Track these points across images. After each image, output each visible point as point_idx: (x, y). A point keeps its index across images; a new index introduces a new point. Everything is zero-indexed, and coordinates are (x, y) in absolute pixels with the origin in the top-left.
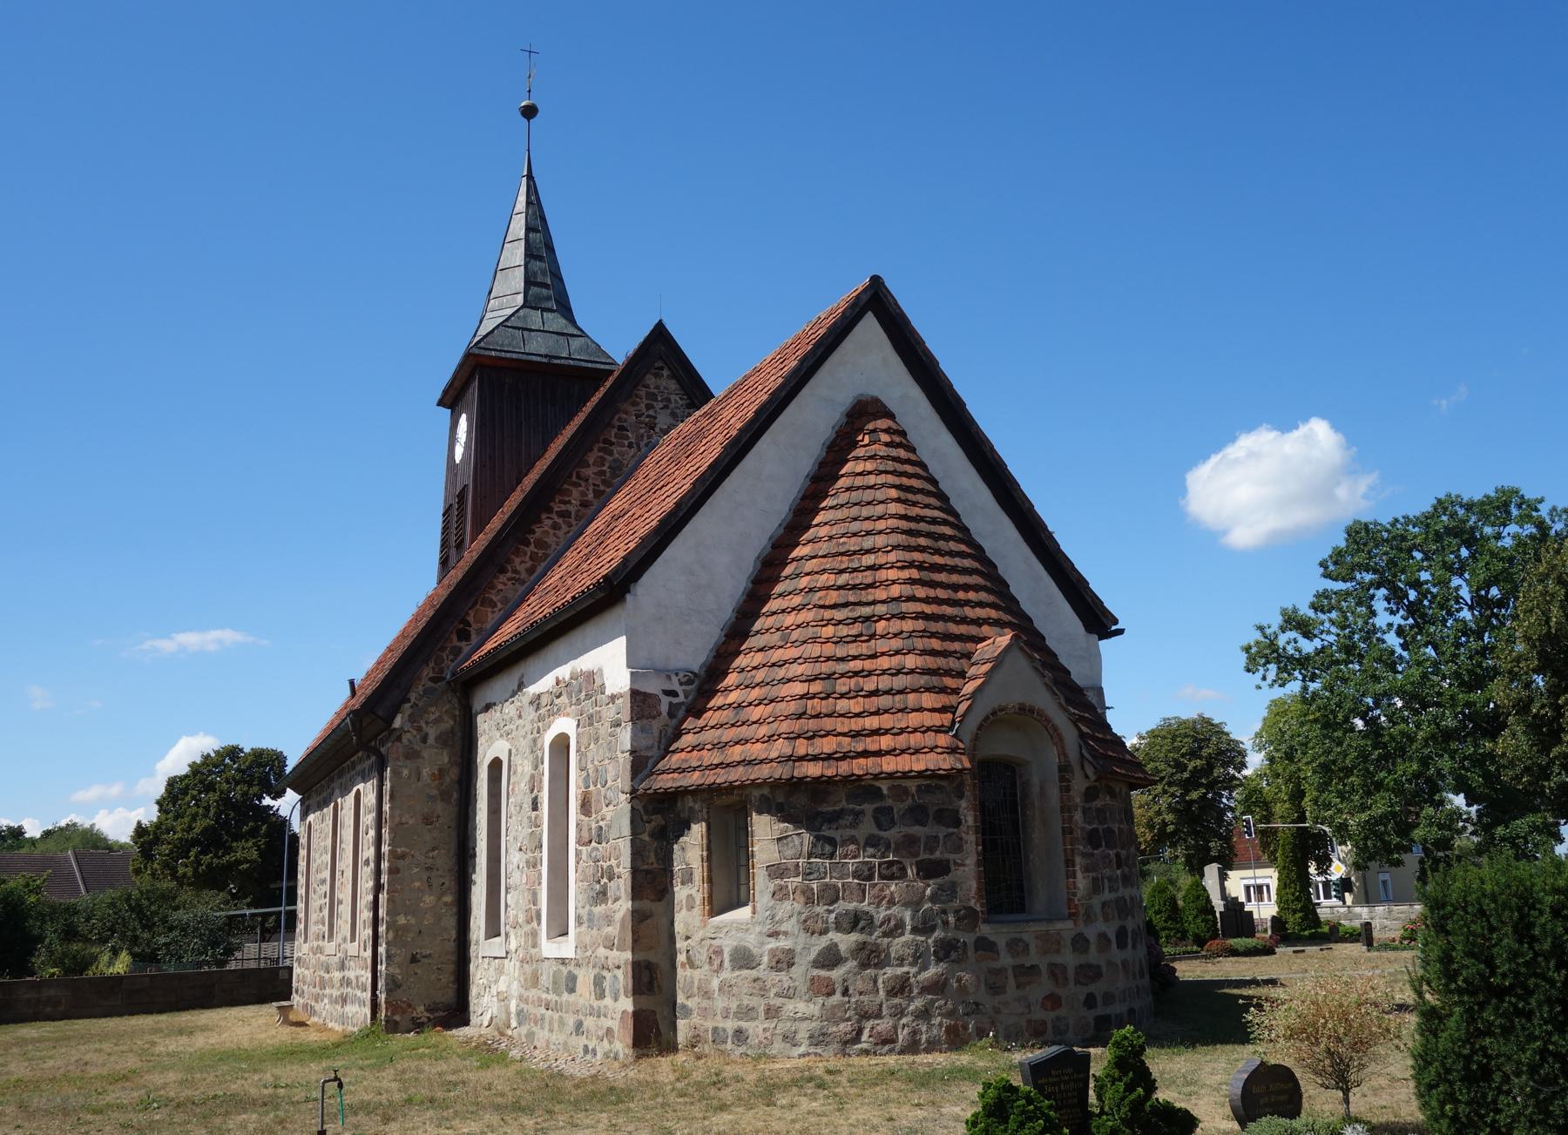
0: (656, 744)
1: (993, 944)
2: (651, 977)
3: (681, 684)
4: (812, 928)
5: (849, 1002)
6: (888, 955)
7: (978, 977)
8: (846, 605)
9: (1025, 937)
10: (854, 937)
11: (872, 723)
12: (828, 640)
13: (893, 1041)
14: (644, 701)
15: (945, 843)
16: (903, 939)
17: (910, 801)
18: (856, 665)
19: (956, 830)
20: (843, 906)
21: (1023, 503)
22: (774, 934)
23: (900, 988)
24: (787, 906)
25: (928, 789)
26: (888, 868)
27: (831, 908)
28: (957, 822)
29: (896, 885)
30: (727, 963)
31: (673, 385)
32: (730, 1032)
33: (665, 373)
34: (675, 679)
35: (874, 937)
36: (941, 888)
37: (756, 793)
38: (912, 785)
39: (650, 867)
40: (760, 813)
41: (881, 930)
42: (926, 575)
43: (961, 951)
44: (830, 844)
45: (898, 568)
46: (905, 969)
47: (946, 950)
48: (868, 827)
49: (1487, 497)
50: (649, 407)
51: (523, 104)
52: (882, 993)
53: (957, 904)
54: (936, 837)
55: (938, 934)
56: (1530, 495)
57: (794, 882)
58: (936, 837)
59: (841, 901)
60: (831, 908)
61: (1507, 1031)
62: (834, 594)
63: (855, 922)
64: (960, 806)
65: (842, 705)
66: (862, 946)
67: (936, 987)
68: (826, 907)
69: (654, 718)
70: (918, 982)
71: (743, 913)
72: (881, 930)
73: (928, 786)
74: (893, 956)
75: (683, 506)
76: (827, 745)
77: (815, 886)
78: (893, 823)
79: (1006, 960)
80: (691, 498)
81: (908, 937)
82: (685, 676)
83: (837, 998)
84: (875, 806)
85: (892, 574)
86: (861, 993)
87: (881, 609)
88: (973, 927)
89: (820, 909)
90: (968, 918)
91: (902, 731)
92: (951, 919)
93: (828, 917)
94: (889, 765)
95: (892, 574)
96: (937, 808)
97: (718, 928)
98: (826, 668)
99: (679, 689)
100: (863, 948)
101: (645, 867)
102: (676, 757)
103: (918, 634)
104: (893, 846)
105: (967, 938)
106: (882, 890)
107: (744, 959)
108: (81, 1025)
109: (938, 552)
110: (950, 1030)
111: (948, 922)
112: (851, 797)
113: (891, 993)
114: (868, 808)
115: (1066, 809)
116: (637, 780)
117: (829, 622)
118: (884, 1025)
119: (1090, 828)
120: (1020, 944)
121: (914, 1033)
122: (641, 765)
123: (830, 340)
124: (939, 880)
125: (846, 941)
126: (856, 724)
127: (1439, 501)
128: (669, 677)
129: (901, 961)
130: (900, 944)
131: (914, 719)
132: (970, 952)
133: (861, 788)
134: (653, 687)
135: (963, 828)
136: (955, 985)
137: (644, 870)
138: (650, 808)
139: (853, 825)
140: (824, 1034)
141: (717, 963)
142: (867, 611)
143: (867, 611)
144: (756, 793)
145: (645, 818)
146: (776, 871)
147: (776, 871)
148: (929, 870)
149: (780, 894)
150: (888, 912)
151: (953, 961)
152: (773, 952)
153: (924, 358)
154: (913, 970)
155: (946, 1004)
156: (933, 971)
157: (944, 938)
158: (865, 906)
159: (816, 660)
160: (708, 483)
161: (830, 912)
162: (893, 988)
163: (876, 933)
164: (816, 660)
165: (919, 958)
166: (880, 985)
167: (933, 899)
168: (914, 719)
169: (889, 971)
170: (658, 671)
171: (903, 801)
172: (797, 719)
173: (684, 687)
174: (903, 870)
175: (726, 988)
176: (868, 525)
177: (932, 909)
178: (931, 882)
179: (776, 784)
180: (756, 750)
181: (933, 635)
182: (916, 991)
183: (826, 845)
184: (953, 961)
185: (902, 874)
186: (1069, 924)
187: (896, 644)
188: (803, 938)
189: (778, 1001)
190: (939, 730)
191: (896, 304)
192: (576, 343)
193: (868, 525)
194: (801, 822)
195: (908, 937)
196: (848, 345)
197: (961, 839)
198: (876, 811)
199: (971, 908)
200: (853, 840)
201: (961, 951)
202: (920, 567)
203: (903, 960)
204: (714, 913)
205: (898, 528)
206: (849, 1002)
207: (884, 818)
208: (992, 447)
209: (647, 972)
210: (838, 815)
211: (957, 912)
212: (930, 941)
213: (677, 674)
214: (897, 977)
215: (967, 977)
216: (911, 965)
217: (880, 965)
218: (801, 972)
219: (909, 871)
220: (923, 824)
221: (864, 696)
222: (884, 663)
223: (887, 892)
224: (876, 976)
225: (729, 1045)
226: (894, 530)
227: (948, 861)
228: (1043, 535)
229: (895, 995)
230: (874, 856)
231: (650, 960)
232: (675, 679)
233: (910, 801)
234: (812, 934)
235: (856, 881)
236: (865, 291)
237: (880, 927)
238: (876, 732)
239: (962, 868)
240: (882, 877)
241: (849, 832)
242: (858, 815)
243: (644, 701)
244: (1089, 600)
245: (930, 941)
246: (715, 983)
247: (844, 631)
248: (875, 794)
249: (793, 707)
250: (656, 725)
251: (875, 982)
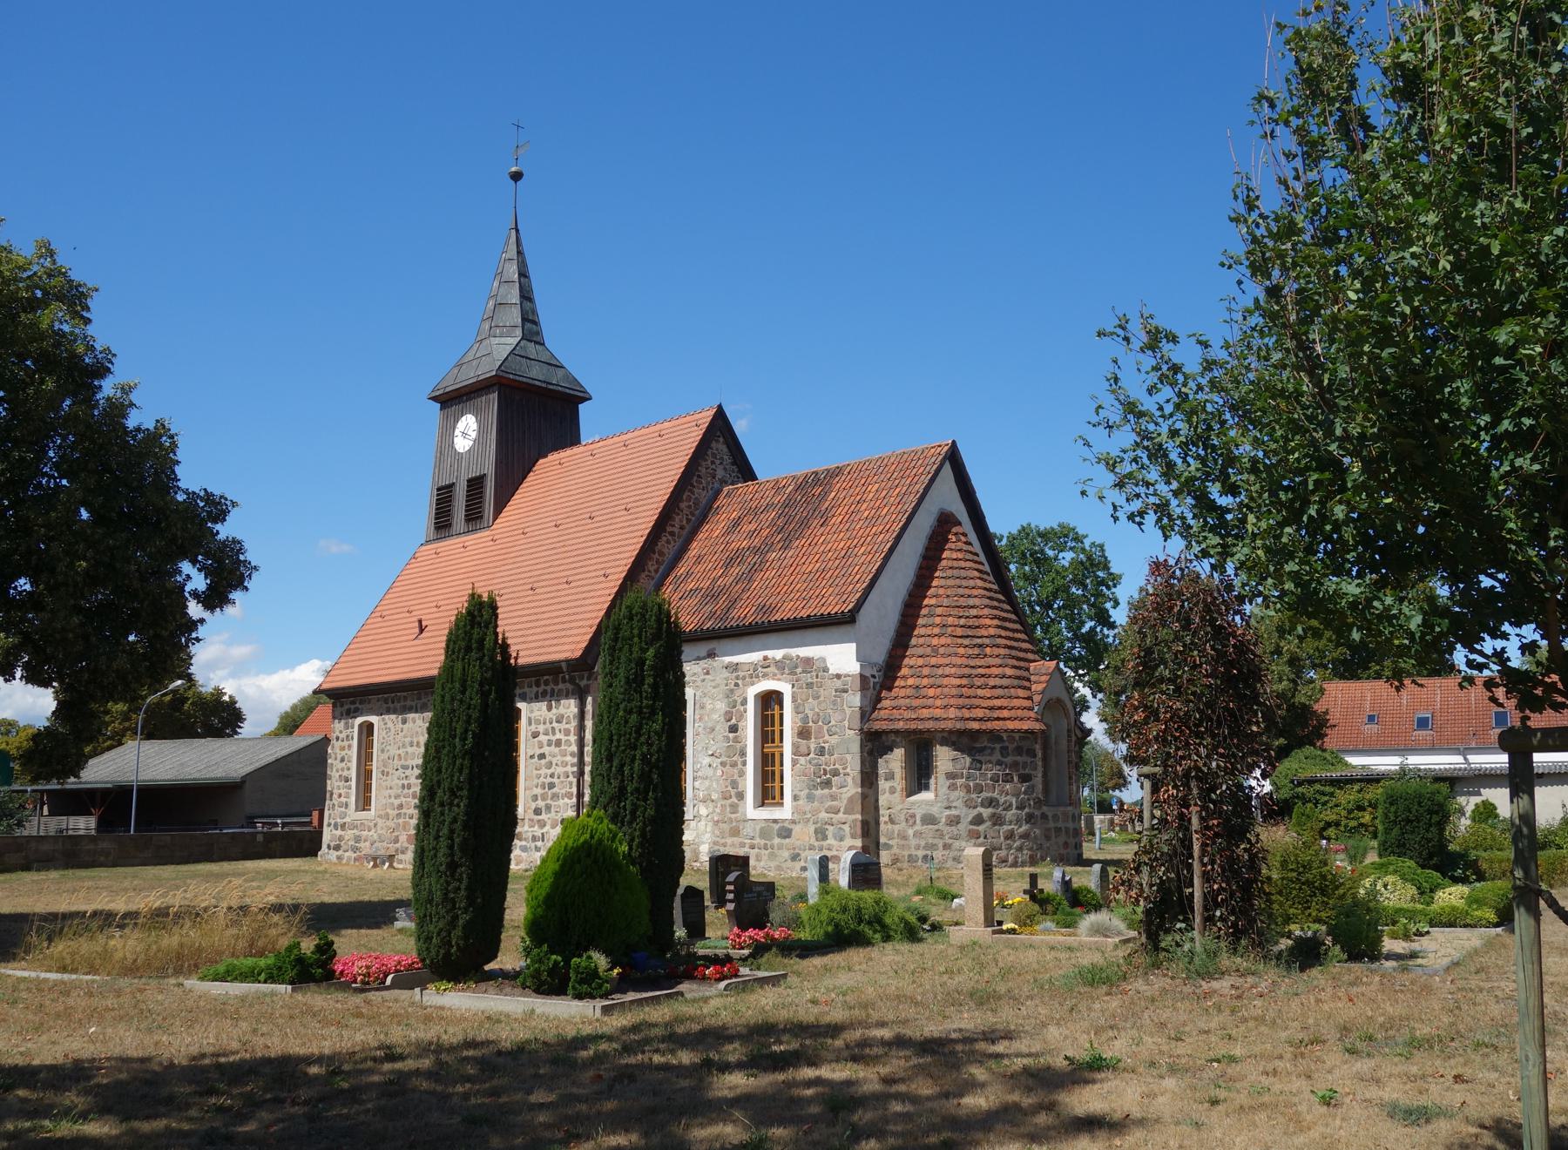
4: (969, 805)
8: (967, 637)
10: (990, 810)
11: (998, 703)
12: (963, 656)
13: (1006, 861)
18: (981, 671)
20: (984, 794)
22: (949, 808)
23: (1010, 836)
24: (956, 793)
28: (1035, 756)
30: (918, 821)
31: (725, 449)
32: (920, 857)
33: (721, 439)
36: (1028, 787)
37: (940, 735)
38: (1017, 736)
40: (941, 745)
47: (1030, 818)
48: (997, 756)
49: (1053, 529)
50: (713, 463)
56: (1081, 531)
57: (960, 782)
61: (1413, 832)
62: (959, 629)
63: (991, 803)
65: (980, 692)
66: (994, 815)
67: (1025, 836)
76: (979, 713)
81: (1014, 811)
85: (988, 622)
87: (987, 641)
88: (1040, 808)
89: (974, 796)
90: (1038, 803)
91: (1013, 708)
94: (1010, 725)
95: (988, 622)
97: (913, 803)
98: (967, 671)
102: (882, 712)
107: (929, 820)
108: (226, 866)
110: (1031, 857)
112: (990, 740)
113: (1007, 838)
114: (998, 746)
117: (961, 645)
118: (1003, 853)
121: (1016, 857)
122: (865, 714)
125: (986, 812)
127: (1023, 528)
129: (1010, 824)
130: (1011, 814)
131: (1016, 703)
133: (994, 736)
139: (990, 755)
141: (911, 822)
142: (979, 641)
143: (979, 641)
144: (940, 735)
146: (950, 776)
147: (950, 776)
148: (1025, 778)
149: (952, 787)
152: (948, 817)
156: (1025, 828)
158: (995, 795)
159: (960, 666)
164: (960, 666)
165: (1018, 821)
167: (1025, 793)
168: (1016, 703)
169: (1006, 828)
175: (917, 834)
176: (967, 592)
179: (951, 732)
180: (938, 713)
181: (1013, 658)
183: (977, 764)
185: (1012, 781)
187: (998, 661)
188: (965, 810)
189: (951, 841)
192: (560, 372)
193: (967, 592)
195: (1014, 811)
200: (990, 762)
204: (909, 795)
215: (1037, 831)
217: (1001, 825)
218: (964, 827)
222: (995, 671)
225: (920, 863)
226: (983, 596)
241: (988, 758)
246: (910, 832)
247: (970, 652)
248: (1000, 739)
249: (954, 691)
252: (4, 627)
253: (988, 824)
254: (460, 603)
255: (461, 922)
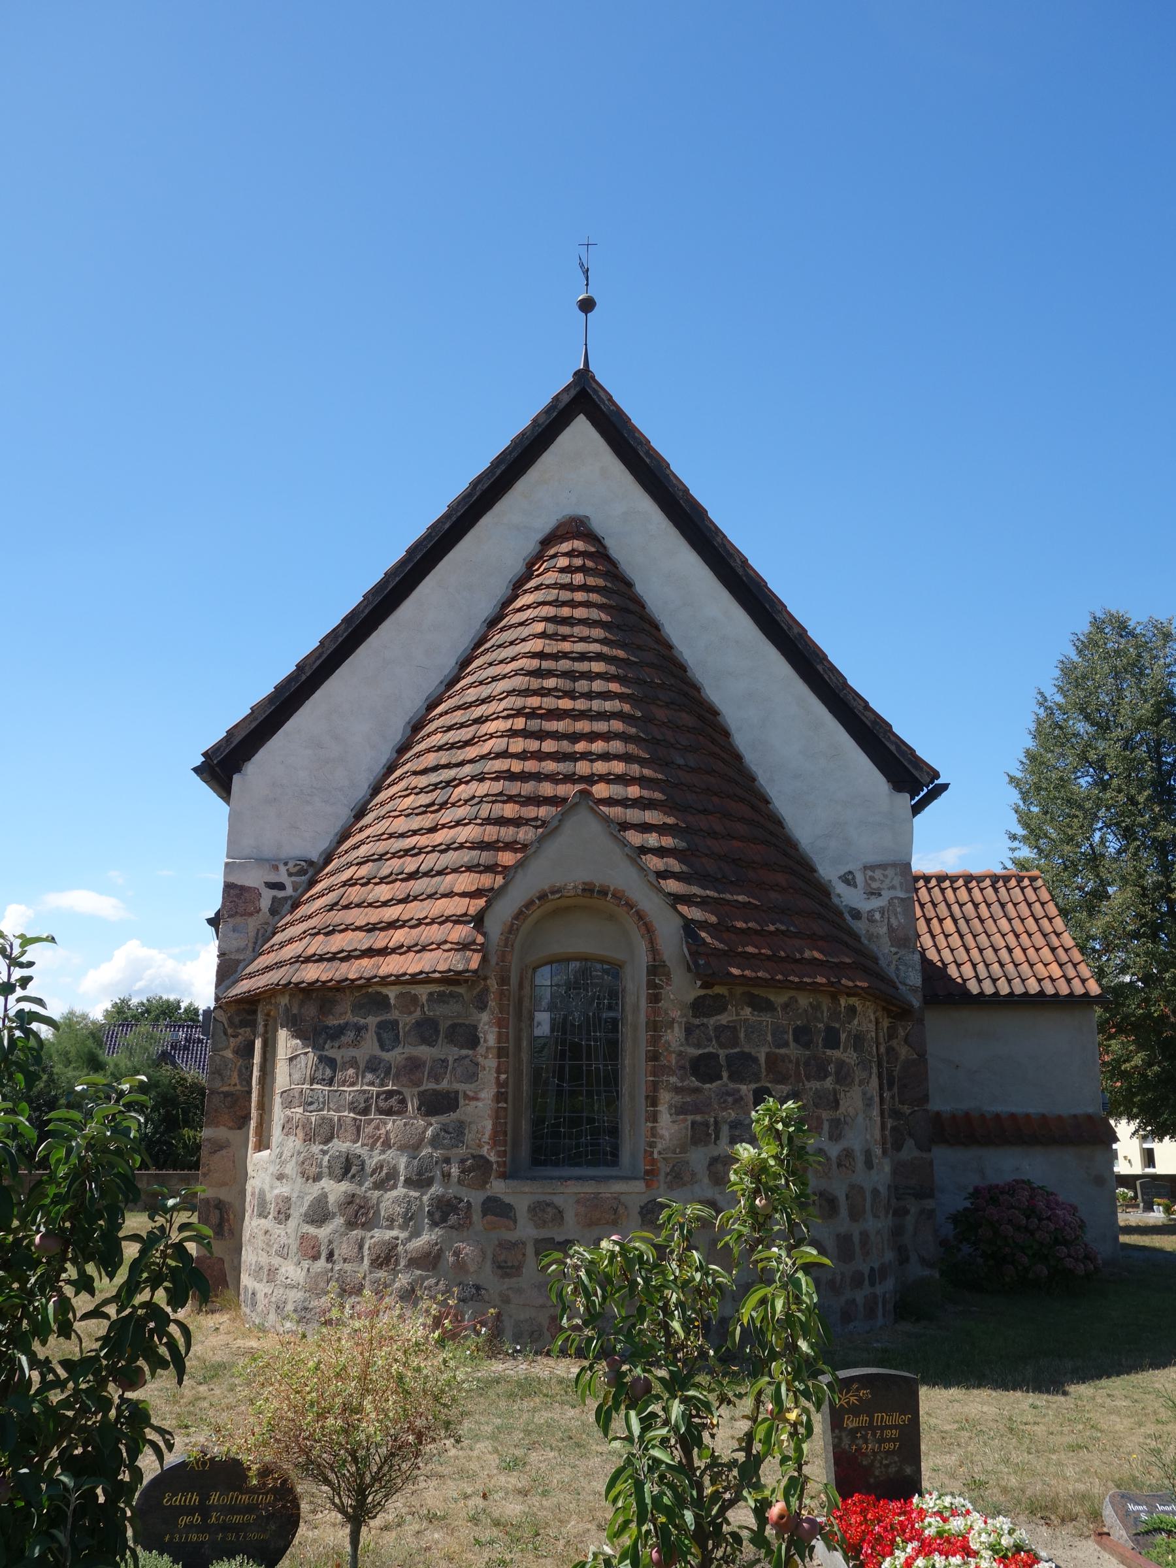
0: (251, 945)
1: (510, 1207)
2: (222, 1218)
3: (290, 875)
5: (332, 1269)
6: (377, 1212)
7: (483, 1252)
9: (558, 1200)
10: (345, 1186)
14: (239, 896)
15: (454, 1069)
16: (394, 1193)
17: (418, 1013)
19: (470, 1052)
20: (340, 1146)
21: (790, 628)
22: (280, 1177)
23: (385, 1258)
25: (441, 998)
26: (386, 1100)
27: (325, 1148)
28: (473, 1041)
29: (394, 1121)
34: (283, 869)
35: (363, 1189)
39: (232, 1089)
41: (372, 1180)
42: (534, 725)
43: (462, 1214)
44: (330, 1068)
45: (503, 718)
46: (395, 1233)
47: (443, 1211)
48: (369, 1047)
51: (580, 298)
52: (366, 1262)
53: (462, 1151)
54: (445, 1061)
55: (436, 1189)
58: (445, 1061)
59: (336, 1140)
60: (325, 1148)
63: (347, 1168)
64: (479, 1021)
66: (350, 1199)
67: (428, 1261)
68: (321, 1147)
69: (251, 914)
70: (406, 1251)
71: (266, 1153)
72: (372, 1180)
73: (441, 994)
74: (382, 1214)
75: (307, 668)
77: (313, 1119)
78: (396, 1041)
79: (526, 1230)
80: (318, 658)
81: (400, 1191)
82: (296, 865)
83: (322, 1263)
84: (379, 1019)
86: (345, 1260)
88: (483, 1183)
89: (316, 1148)
90: (479, 1169)
92: (455, 1171)
93: (322, 1159)
94: (391, 965)
96: (450, 1022)
99: (288, 881)
100: (350, 1203)
101: (225, 1089)
103: (490, 798)
104: (393, 1071)
105: (475, 1197)
106: (377, 1128)
109: (571, 695)
111: (449, 1175)
112: (358, 1008)
114: (372, 1021)
115: (655, 1027)
116: (222, 987)
119: (695, 1052)
120: (549, 1209)
123: (515, 454)
124: (443, 1118)
125: (335, 1190)
126: (374, 916)
128: (276, 868)
130: (392, 1200)
132: (476, 1216)
134: (253, 878)
135: (481, 1050)
136: (451, 1259)
137: (223, 1092)
138: (237, 1020)
139: (355, 1044)
140: (306, 1309)
145: (230, 1031)
150: (382, 1157)
151: (452, 1227)
153: (648, 460)
154: (403, 1235)
155: (437, 1284)
156: (427, 1238)
157: (443, 1196)
158: (358, 1148)
160: (340, 640)
161: (324, 1153)
162: (379, 1257)
163: (367, 1184)
165: (410, 1219)
166: (366, 1252)
167: (435, 1142)
169: (377, 1233)
170: (260, 861)
171: (411, 1013)
172: (329, 911)
173: (293, 879)
174: (403, 1102)
177: (432, 1156)
178: (433, 1120)
181: (510, 799)
182: (403, 1263)
184: (452, 1227)
186: (639, 1186)
190: (458, 920)
191: (610, 398)
194: (308, 1039)
195: (400, 1191)
196: (548, 460)
197: (477, 1064)
198: (381, 1026)
199: (482, 1157)
200: (353, 1063)
201: (462, 1214)
202: (532, 714)
203: (393, 1221)
205: (522, 669)
206: (332, 1269)
207: (389, 1034)
208: (745, 561)
209: (217, 1212)
210: (341, 1030)
211: (463, 1161)
212: (425, 1198)
213: (286, 864)
214: (384, 1243)
216: (402, 1228)
217: (368, 1226)
219: (410, 1105)
220: (430, 1043)
221: (402, 880)
223: (383, 1131)
224: (363, 1239)
227: (457, 1092)
228: (820, 668)
229: (380, 1266)
230: (372, 1084)
231: (221, 1198)
232: (283, 869)
233: (418, 1013)
234: (307, 1180)
235: (352, 1115)
236: (567, 389)
237: (372, 1176)
238: (393, 925)
239: (473, 1103)
240: (381, 1111)
242: (360, 1029)
243: (239, 896)
244: (893, 748)
245: (425, 1198)
248: (381, 1003)
250: (253, 924)
251: (361, 1247)
252: (1172, 788)
253: (339, 1221)
254: (196, 779)
255: (697, 1084)
